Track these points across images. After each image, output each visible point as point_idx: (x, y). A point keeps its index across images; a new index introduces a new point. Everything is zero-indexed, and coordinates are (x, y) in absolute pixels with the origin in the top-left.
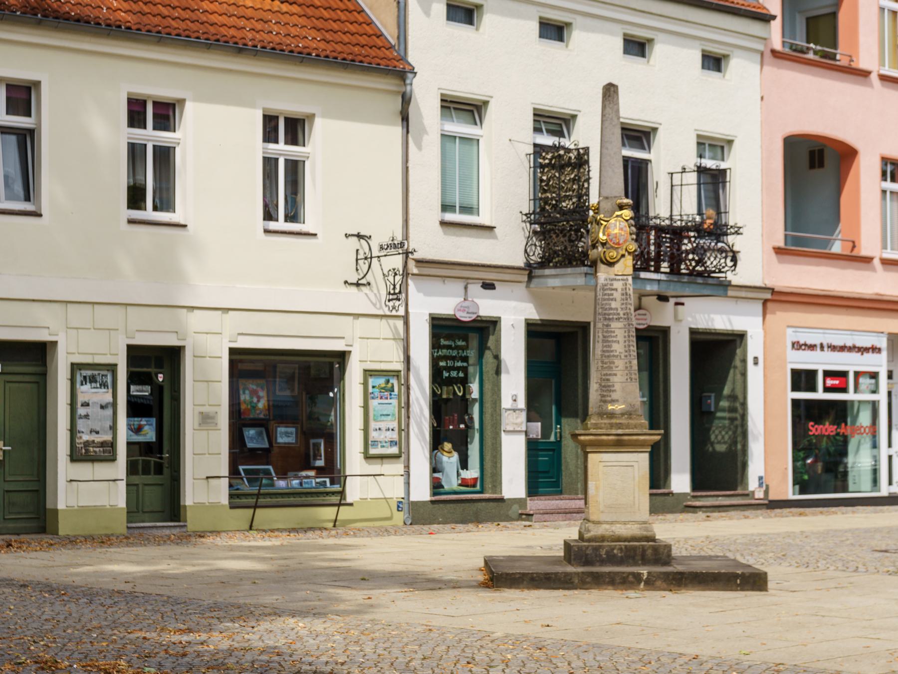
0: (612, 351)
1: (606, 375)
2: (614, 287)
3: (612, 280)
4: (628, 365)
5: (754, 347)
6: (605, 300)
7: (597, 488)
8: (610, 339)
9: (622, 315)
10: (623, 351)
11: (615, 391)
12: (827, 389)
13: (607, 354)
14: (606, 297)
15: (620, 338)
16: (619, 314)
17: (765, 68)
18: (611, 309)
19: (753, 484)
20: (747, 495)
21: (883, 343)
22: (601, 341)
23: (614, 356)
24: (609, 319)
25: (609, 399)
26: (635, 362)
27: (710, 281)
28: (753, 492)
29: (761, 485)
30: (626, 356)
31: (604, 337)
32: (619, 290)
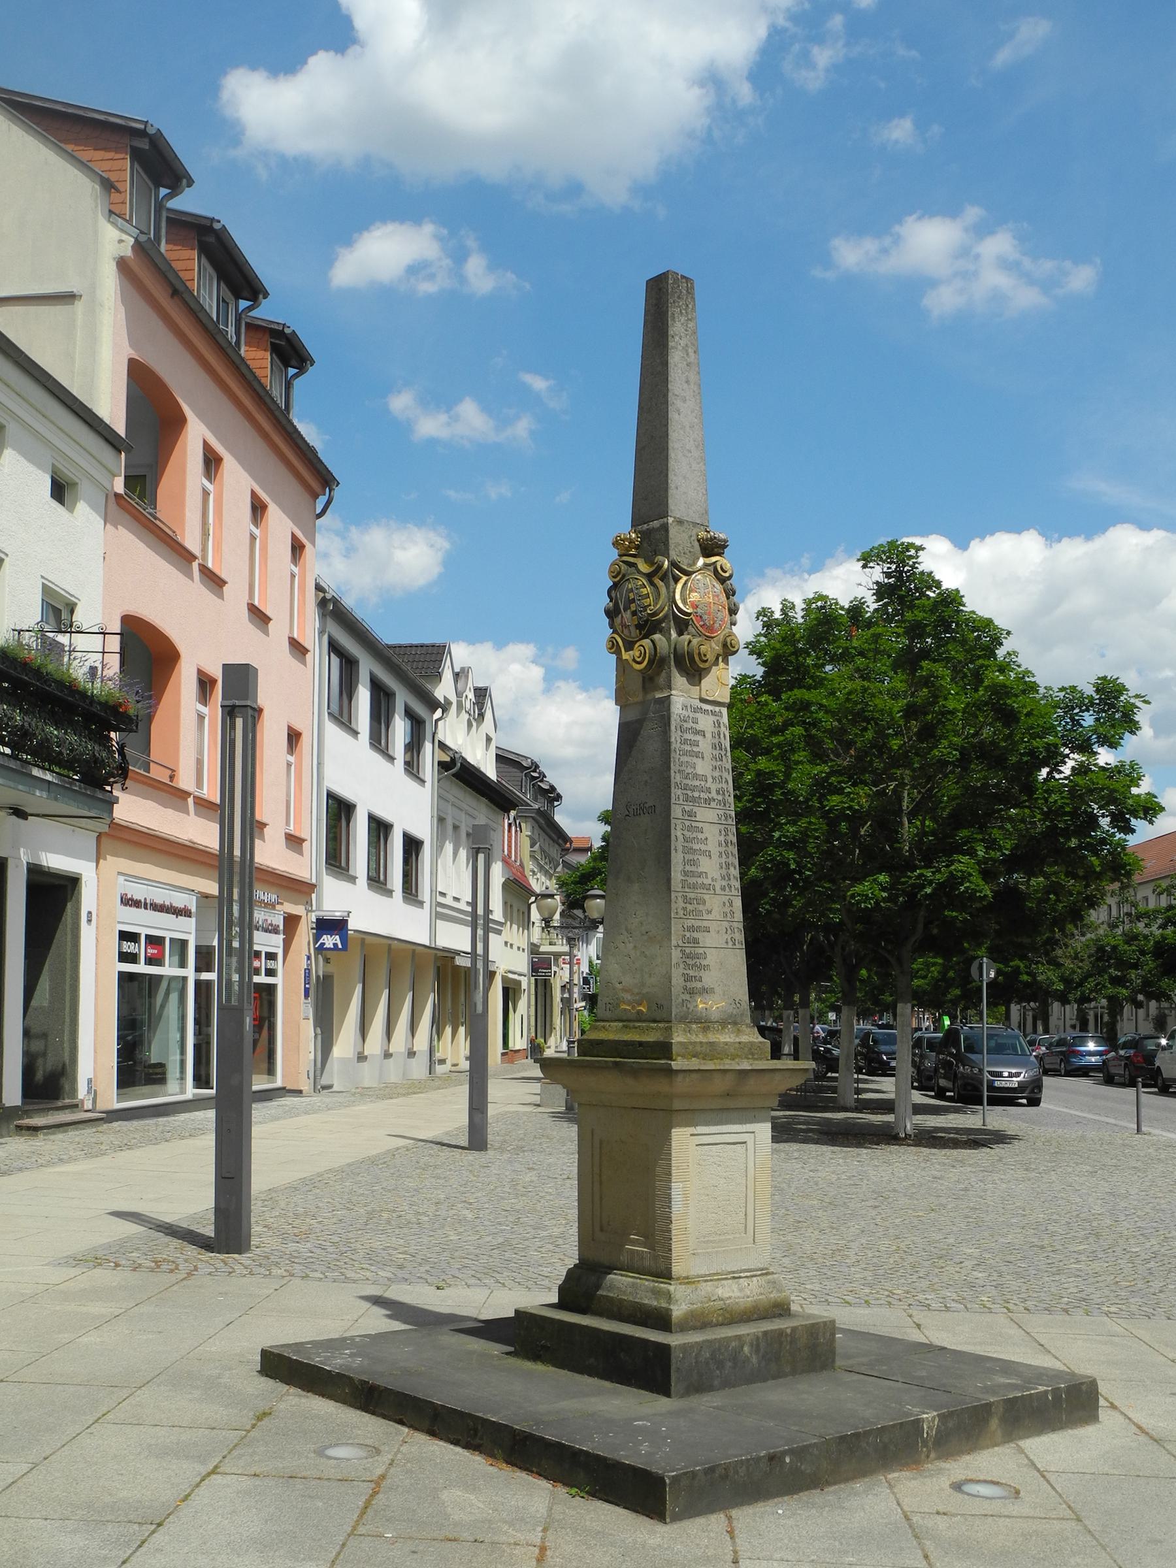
0: (700, 875)
1: (692, 929)
2: (699, 727)
3: (696, 710)
4: (727, 909)
5: (88, 898)
6: (686, 753)
7: (686, 1198)
8: (696, 847)
9: (714, 794)
10: (717, 875)
11: (706, 968)
12: (183, 964)
13: (691, 880)
14: (688, 748)
15: (712, 846)
16: (709, 790)
17: (108, 525)
18: (696, 776)
19: (82, 1091)
20: (76, 1106)
21: (191, 903)
22: (680, 849)
23: (703, 886)
24: (694, 800)
25: (699, 985)
26: (738, 903)
27: (99, 795)
28: (82, 1101)
29: (89, 1089)
30: (723, 889)
31: (686, 840)
32: (709, 735)
